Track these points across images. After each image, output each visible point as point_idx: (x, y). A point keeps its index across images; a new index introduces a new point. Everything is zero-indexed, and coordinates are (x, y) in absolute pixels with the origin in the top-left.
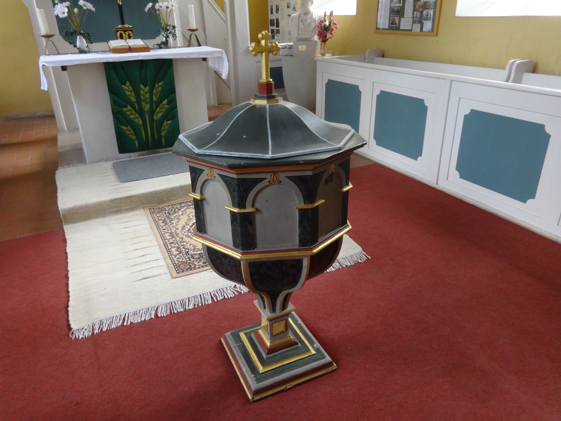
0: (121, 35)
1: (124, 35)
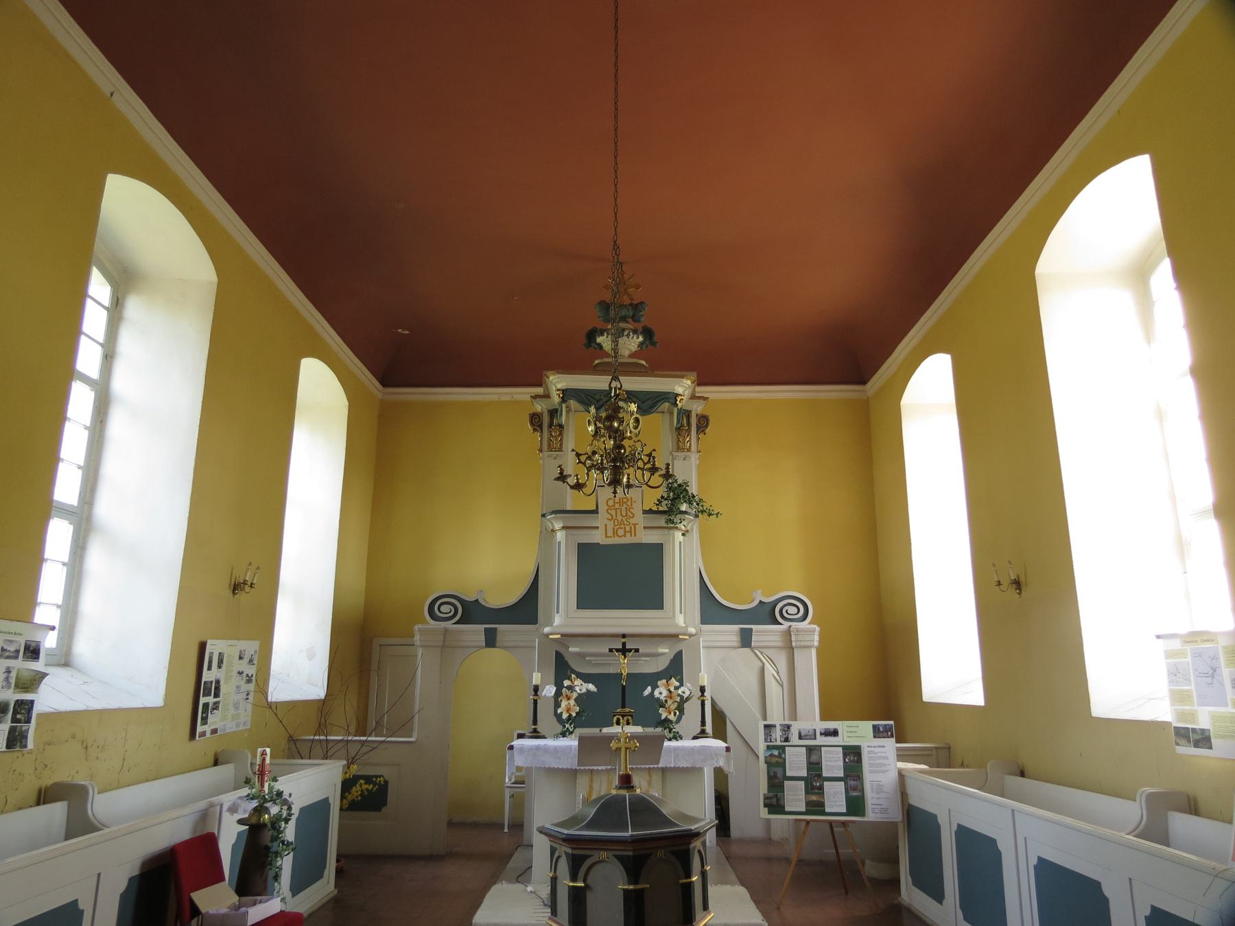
0: (618, 720)
1: (621, 721)
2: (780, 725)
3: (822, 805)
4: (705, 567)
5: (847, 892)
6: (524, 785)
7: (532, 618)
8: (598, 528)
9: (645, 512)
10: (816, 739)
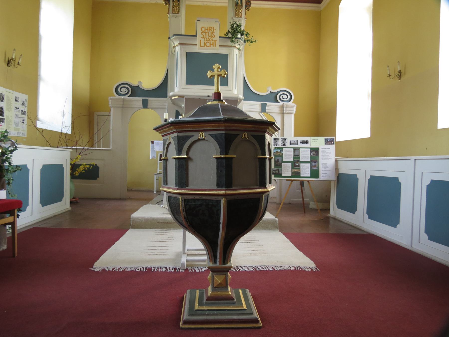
2: (281, 138)
3: (299, 173)
4: (246, 75)
5: (305, 213)
6: (161, 174)
7: (165, 95)
8: (196, 45)
9: (220, 37)
10: (297, 145)
